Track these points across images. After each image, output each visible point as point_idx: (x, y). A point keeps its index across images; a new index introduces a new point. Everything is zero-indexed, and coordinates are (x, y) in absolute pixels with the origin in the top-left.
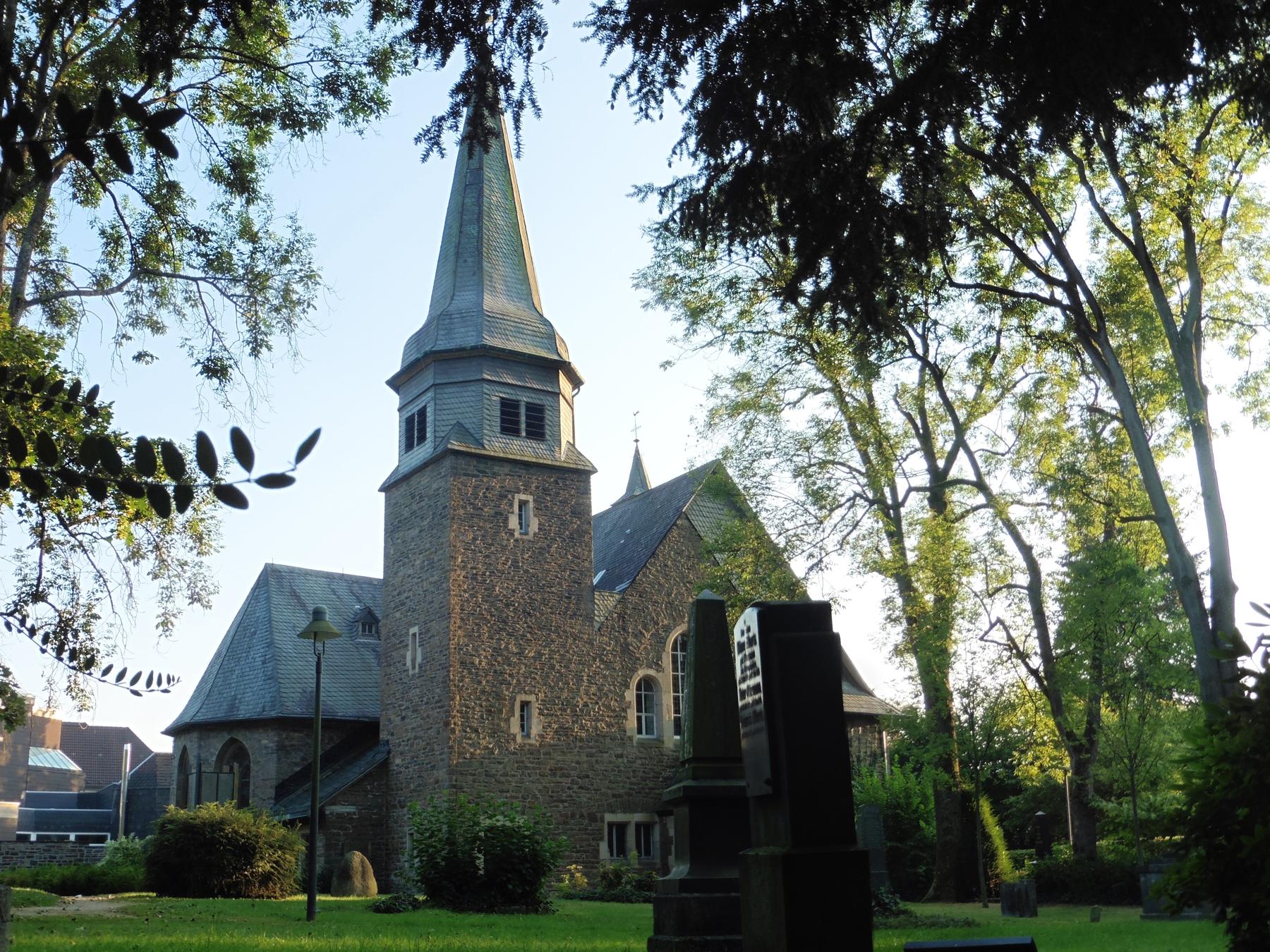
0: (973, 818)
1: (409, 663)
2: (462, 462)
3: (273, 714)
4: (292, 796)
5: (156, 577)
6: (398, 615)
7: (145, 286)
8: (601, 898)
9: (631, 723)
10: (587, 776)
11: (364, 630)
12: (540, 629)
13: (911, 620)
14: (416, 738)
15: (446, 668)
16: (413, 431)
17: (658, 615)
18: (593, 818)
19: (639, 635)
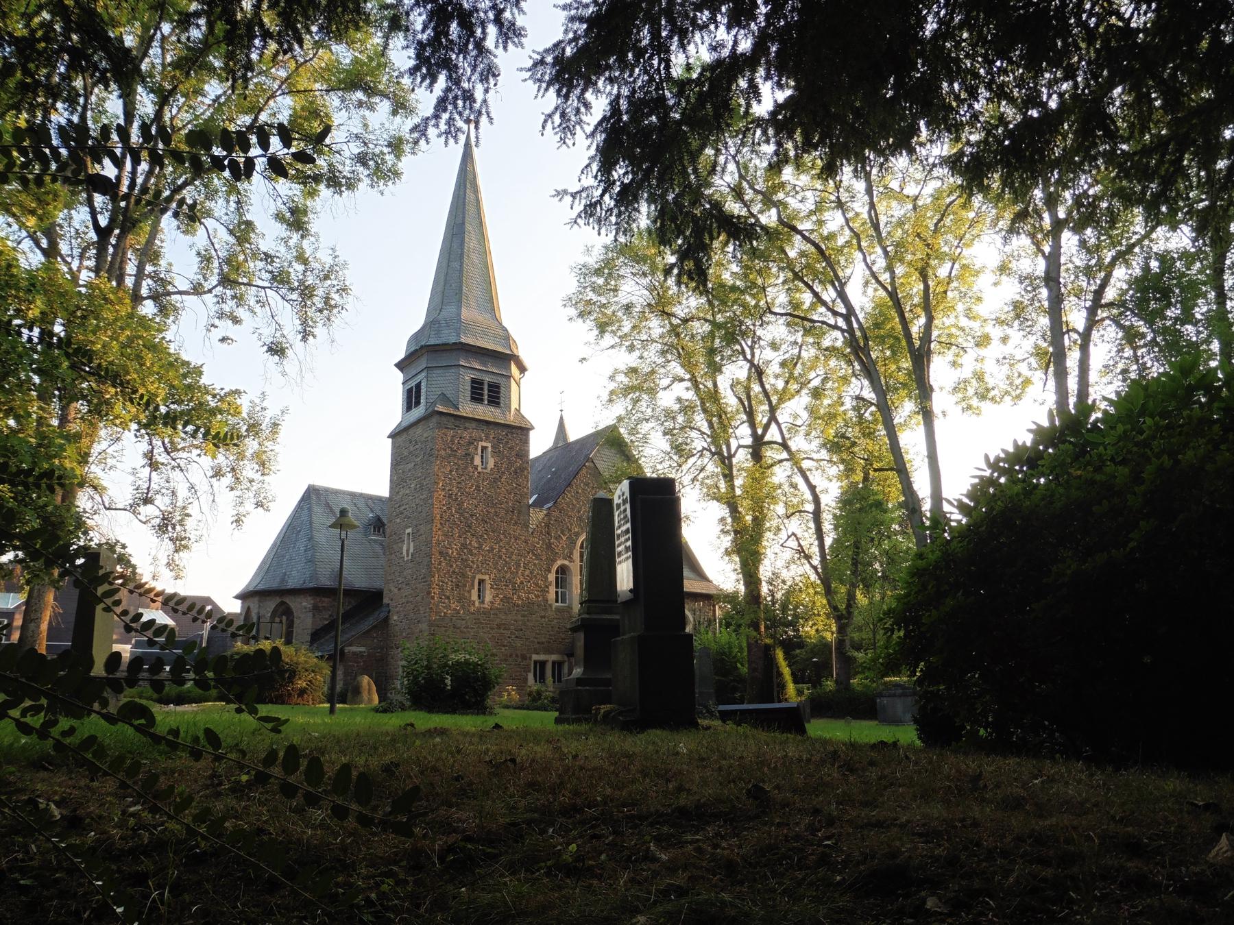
0: (771, 662)
2: (444, 419)
3: (311, 585)
5: (232, 489)
7: (228, 292)
8: (528, 708)
9: (552, 596)
13: (736, 532)
16: (412, 398)
19: (558, 538)
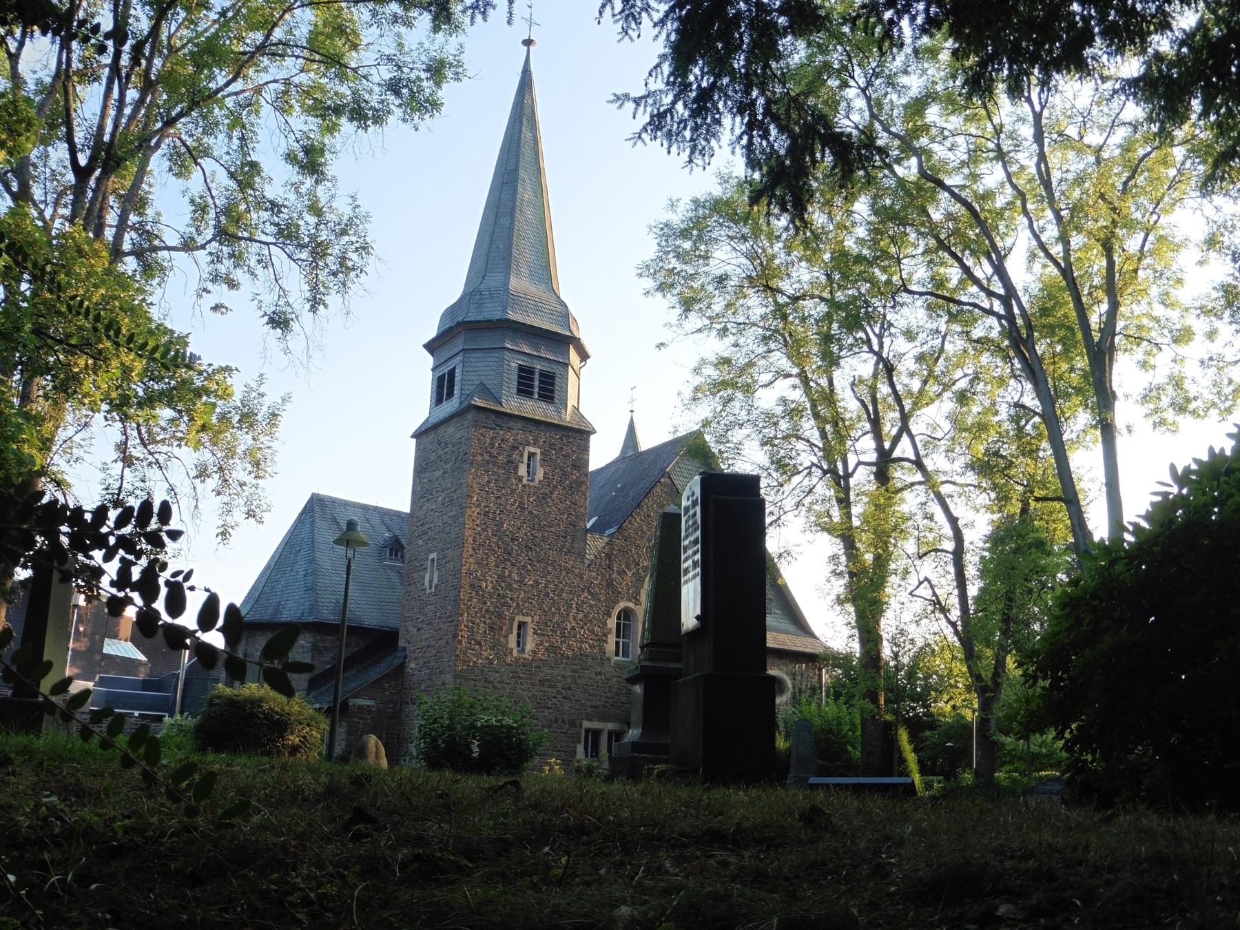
2: (482, 415)
3: (310, 619)
4: (323, 689)
5: (219, 494)
6: (420, 542)
9: (611, 646)
10: (570, 689)
12: (539, 562)
13: (852, 575)
14: (428, 646)
15: (458, 589)
16: (443, 387)
17: (639, 557)
18: (573, 724)
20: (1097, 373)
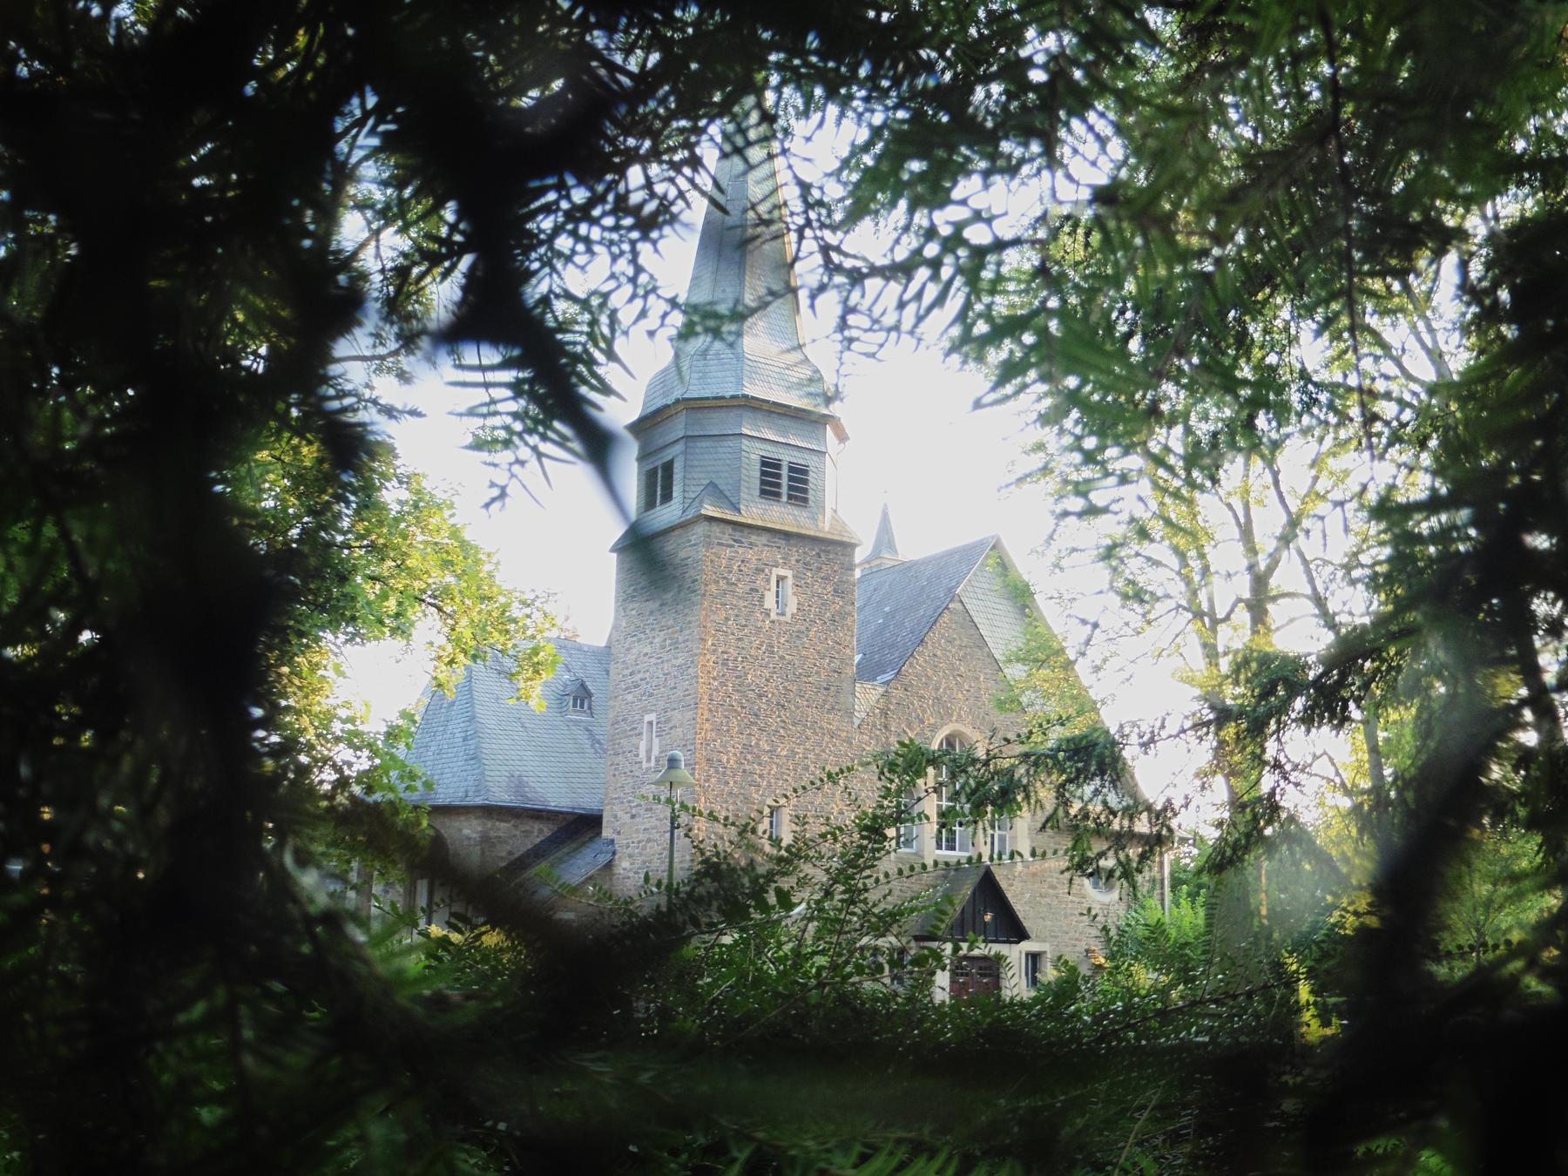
1: (643, 754)
2: (716, 528)
3: (479, 801)
6: (630, 697)
11: (575, 705)
14: (649, 840)
17: (924, 711)
20: (1546, 726)
